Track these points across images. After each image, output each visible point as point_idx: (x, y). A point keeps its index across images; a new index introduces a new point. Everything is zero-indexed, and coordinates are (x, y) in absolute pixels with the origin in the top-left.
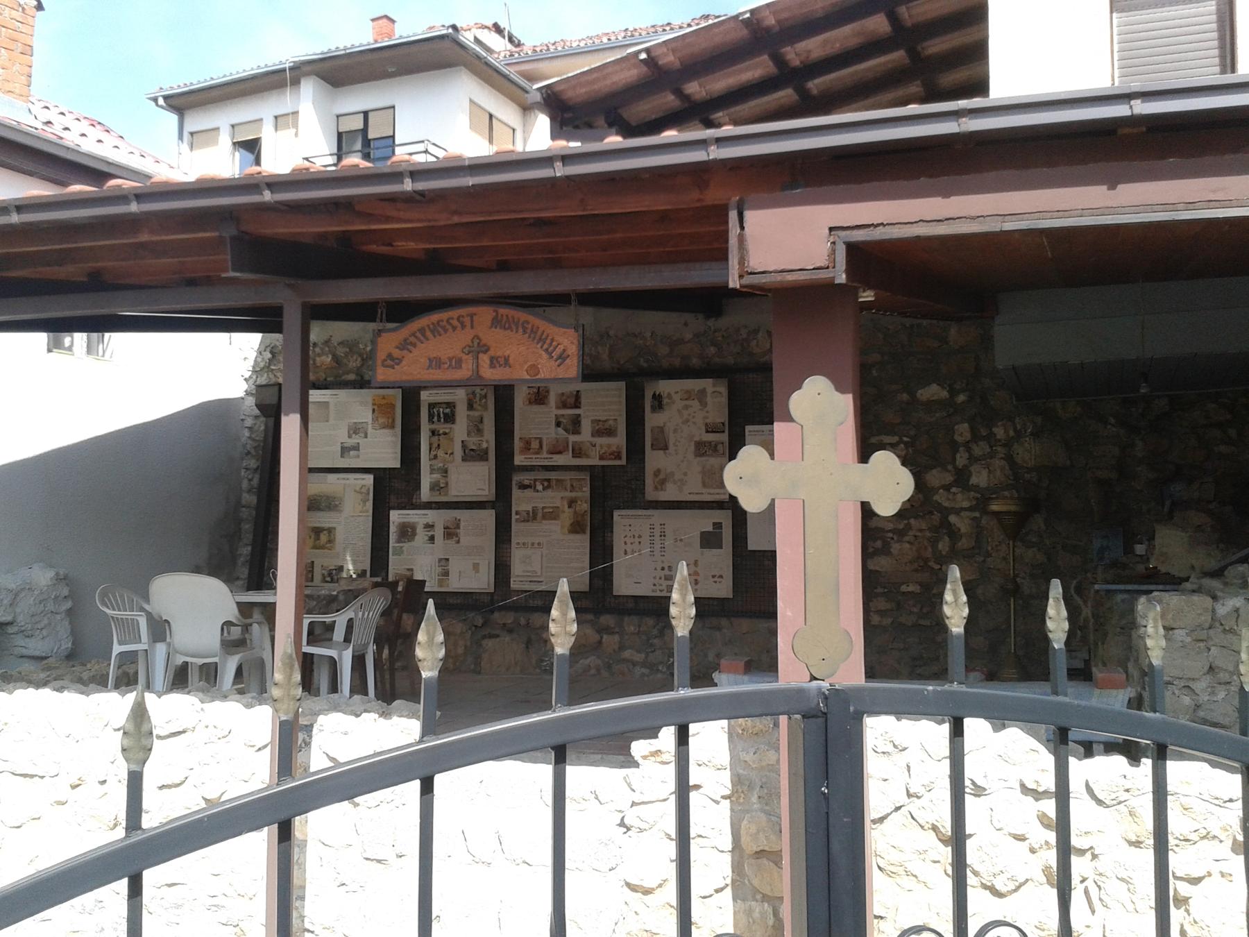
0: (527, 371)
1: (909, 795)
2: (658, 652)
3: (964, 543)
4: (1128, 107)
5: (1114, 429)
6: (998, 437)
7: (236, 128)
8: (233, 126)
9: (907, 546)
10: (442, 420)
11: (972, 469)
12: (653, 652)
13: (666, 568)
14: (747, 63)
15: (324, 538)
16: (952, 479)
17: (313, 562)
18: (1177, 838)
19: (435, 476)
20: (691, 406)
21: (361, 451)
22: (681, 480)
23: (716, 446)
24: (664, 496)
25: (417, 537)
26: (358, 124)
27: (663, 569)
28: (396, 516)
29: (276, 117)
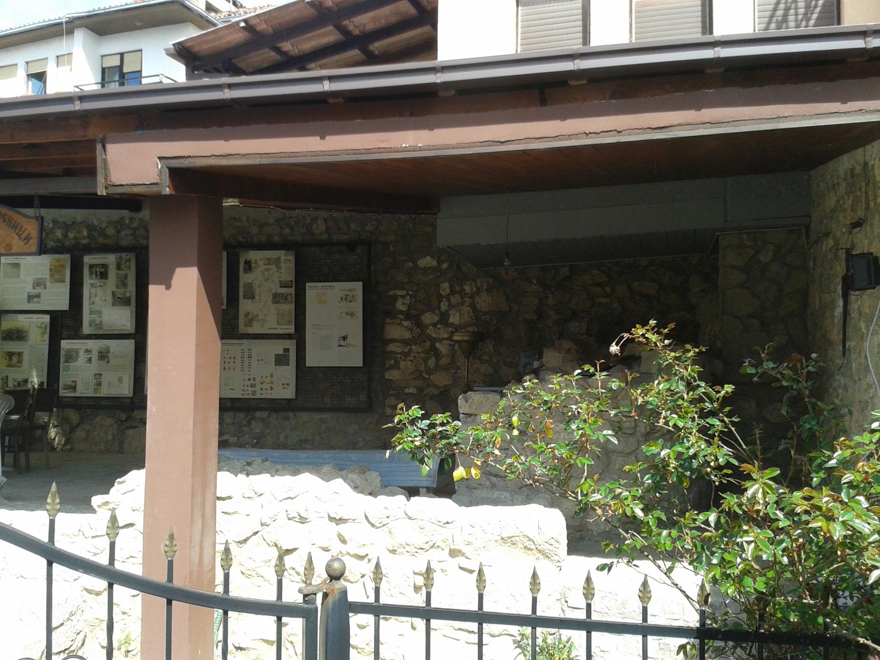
0: (5, 248)
1: (262, 525)
2: (247, 436)
3: (444, 361)
4: (435, 77)
5: (535, 287)
6: (466, 292)
7: (29, 64)
8: (27, 63)
9: (409, 363)
10: (99, 277)
11: (450, 313)
12: (242, 436)
13: (252, 379)
14: (310, 35)
15: (15, 359)
16: (437, 319)
17: (7, 376)
18: (416, 548)
19: (93, 316)
20: (270, 269)
21: (42, 298)
22: (263, 320)
23: (287, 296)
24: (250, 330)
25: (79, 359)
26: (116, 62)
27: (249, 380)
28: (65, 344)
29: (58, 57)
